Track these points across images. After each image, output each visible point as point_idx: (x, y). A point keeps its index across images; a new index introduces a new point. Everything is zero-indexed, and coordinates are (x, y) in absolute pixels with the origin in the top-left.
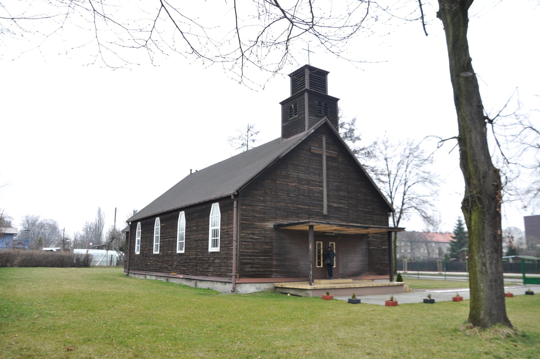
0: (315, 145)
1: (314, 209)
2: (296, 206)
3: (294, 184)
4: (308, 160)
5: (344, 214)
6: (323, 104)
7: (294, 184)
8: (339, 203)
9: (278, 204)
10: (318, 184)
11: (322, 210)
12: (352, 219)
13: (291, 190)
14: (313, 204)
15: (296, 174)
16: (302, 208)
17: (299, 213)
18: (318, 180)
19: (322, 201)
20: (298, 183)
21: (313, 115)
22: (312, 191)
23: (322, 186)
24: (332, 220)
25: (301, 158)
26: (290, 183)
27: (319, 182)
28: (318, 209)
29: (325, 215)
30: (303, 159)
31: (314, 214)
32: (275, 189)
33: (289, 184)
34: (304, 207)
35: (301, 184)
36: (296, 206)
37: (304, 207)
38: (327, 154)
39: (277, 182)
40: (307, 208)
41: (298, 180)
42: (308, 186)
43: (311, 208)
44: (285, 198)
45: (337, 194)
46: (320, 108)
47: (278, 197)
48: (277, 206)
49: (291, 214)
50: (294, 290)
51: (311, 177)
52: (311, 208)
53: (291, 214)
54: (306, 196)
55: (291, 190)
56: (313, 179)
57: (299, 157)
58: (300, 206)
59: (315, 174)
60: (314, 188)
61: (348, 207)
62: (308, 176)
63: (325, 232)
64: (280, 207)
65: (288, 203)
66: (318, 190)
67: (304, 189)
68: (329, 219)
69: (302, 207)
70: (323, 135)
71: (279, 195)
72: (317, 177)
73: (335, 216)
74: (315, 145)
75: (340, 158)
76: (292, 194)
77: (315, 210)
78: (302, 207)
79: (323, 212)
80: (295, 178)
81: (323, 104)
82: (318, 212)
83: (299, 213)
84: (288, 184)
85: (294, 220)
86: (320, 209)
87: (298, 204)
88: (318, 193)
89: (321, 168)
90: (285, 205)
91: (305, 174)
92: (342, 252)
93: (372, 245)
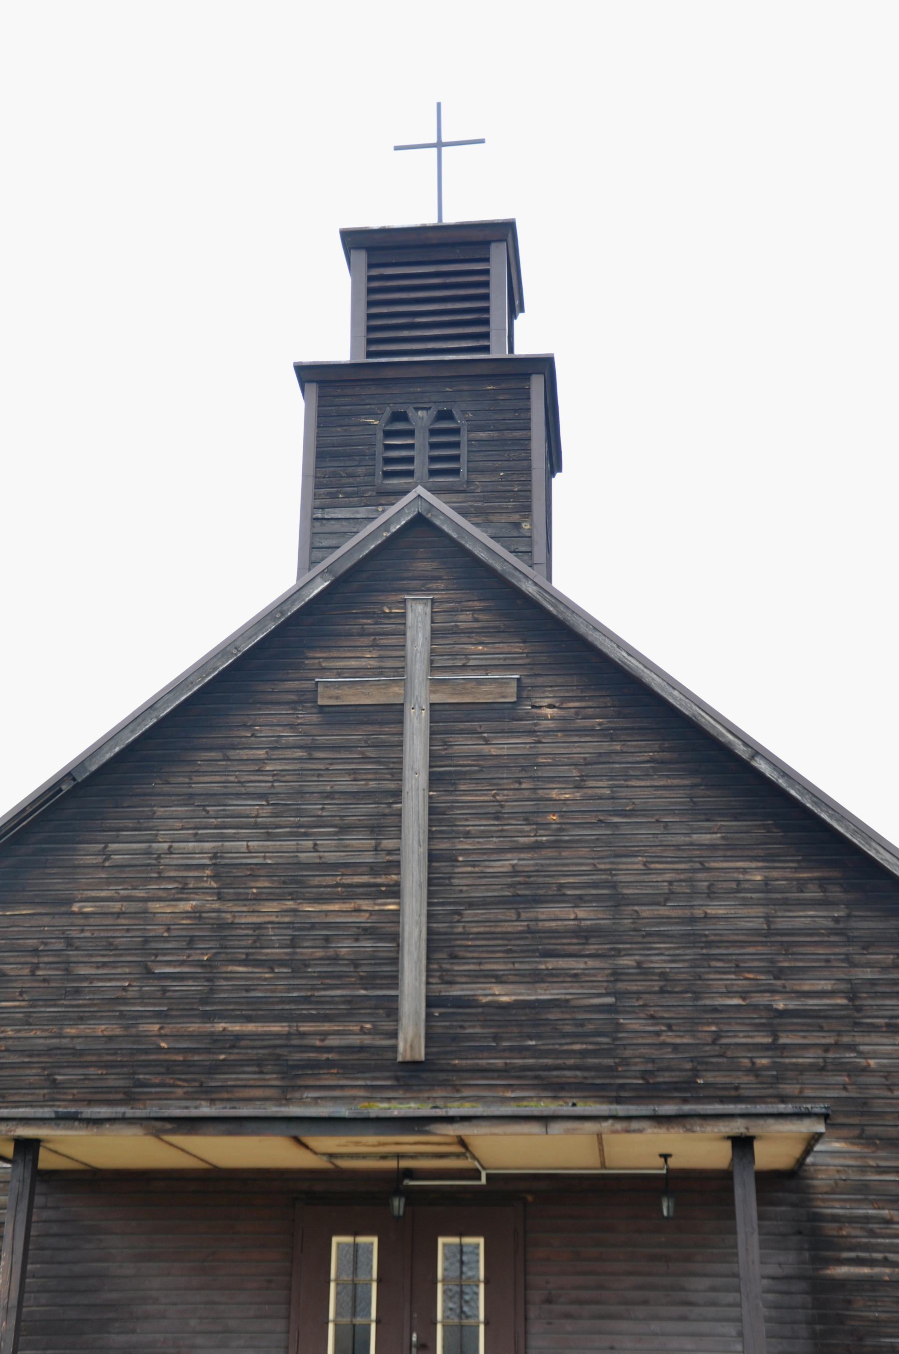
0: (354, 663)
1: (325, 1035)
2: (194, 1027)
3: (187, 906)
4: (299, 753)
5: (577, 1047)
6: (422, 418)
7: (187, 906)
8: (537, 978)
9: (71, 1031)
10: (364, 879)
11: (394, 1035)
12: (644, 1074)
13: (166, 940)
14: (320, 1002)
15: (208, 846)
16: (239, 1037)
17: (215, 1068)
18: (368, 858)
19: (394, 980)
20: (220, 898)
21: (348, 495)
22: (313, 926)
23: (395, 892)
24: (466, 1093)
25: (244, 754)
26: (160, 900)
27: (373, 869)
28: (363, 1032)
29: (412, 1065)
30: (261, 753)
31: (329, 1064)
32: (60, 945)
33: (155, 906)
34: (250, 1027)
35: (239, 898)
36: (194, 1027)
37: (250, 1027)
38: (437, 698)
39: (75, 908)
40: (278, 1035)
41: (215, 877)
42: (290, 904)
43: (305, 1027)
44: (124, 989)
45: (521, 926)
46: (388, 447)
47: (77, 991)
48: (65, 1041)
49: (157, 1080)
50: (646, 1047)
51: (315, 848)
52: (305, 1027)
53: (157, 1080)
54: (270, 964)
55: (166, 940)
56: (331, 857)
57: (233, 747)
58: (220, 1026)
59: (344, 829)
60: (336, 907)
61: (610, 1000)
62: (290, 844)
63: (410, 1173)
64: (79, 1044)
65: (141, 1016)
66: (363, 918)
67: (259, 926)
68: (443, 1084)
69: (236, 1028)
70: (408, 591)
71: (85, 978)
72: (360, 842)
73: (499, 1062)
74: (354, 663)
75: (546, 702)
76: (168, 963)
77: (332, 1041)
78: (236, 1028)
79: (394, 1048)
80: (203, 866)
81: (422, 418)
82: (362, 1048)
83: (215, 1068)
84: (146, 912)
85: (558, 1077)
86: (375, 1032)
87: (209, 1017)
88: (368, 932)
89: (391, 786)
90: (118, 1031)
91: (269, 837)
92: (549, 1301)
93: (846, 1255)
